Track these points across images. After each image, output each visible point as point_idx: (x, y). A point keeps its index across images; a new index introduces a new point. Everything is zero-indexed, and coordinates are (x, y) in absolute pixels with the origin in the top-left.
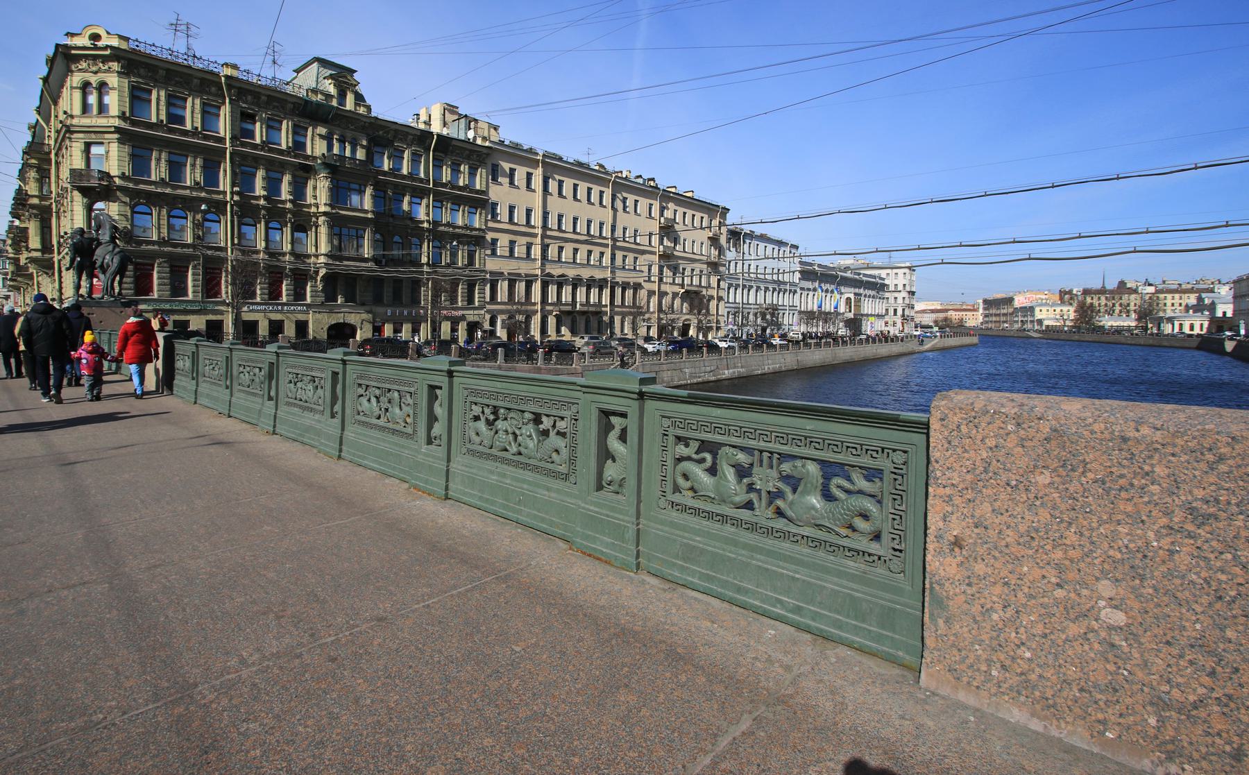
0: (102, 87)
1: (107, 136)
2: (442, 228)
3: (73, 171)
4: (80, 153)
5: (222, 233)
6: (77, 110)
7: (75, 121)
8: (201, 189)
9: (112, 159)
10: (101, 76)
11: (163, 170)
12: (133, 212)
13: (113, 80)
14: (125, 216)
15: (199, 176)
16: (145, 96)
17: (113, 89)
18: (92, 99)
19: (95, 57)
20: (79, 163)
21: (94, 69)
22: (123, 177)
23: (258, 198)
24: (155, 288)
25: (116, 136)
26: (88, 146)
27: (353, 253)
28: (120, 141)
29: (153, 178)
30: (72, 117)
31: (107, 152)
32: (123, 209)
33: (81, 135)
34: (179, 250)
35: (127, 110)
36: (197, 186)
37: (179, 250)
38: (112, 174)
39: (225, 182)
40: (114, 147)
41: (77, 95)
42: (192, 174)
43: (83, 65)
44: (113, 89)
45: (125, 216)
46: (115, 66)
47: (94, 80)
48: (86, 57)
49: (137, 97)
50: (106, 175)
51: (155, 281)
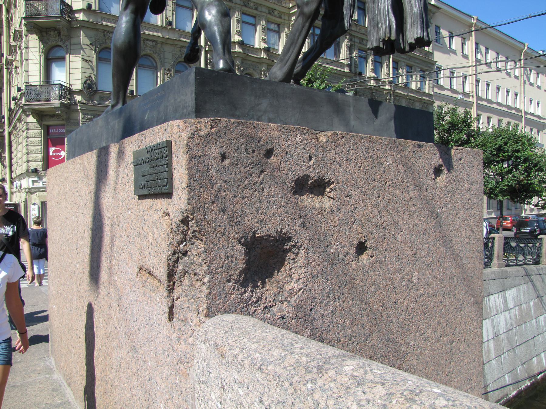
38: (75, 8)
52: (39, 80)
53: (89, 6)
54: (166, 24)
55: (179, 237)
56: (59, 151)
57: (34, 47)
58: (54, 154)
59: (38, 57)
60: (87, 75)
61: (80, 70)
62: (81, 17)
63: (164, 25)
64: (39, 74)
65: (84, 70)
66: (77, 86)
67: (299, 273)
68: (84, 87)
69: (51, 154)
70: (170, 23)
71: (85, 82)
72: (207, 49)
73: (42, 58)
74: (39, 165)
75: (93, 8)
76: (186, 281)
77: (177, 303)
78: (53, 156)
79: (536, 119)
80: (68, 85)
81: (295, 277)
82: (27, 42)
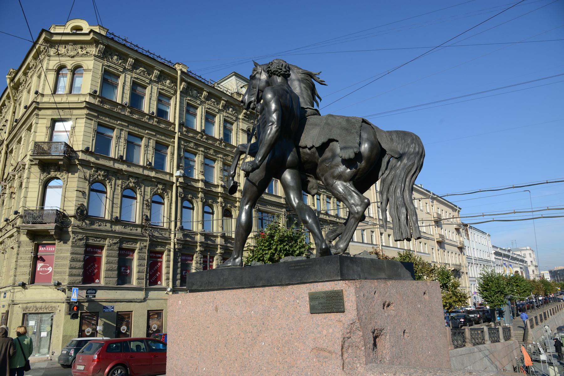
0: (76, 69)
1: (75, 112)
2: (321, 216)
3: (37, 145)
4: (45, 130)
5: (165, 214)
6: (48, 91)
7: (45, 99)
8: (152, 169)
9: (74, 133)
10: (78, 60)
11: (121, 148)
12: (91, 190)
13: (89, 63)
14: (84, 193)
15: (151, 157)
16: (113, 80)
17: (88, 70)
18: (64, 82)
19: (75, 43)
20: (41, 135)
21: (72, 54)
22: (87, 151)
23: (197, 181)
24: (103, 274)
25: (86, 111)
26: (54, 121)
27: (389, 246)
28: (89, 117)
29: (112, 155)
30: (43, 95)
31: (73, 128)
32: (81, 185)
33: (49, 112)
34: (128, 230)
35: (98, 90)
36: (149, 167)
37: (128, 230)
38: (75, 149)
39: (171, 165)
40: (82, 124)
41: (51, 77)
42: (144, 155)
43: (62, 50)
44: (88, 70)
45: (84, 193)
46: (93, 50)
47: (70, 63)
48: (66, 43)
49: (108, 79)
50: (69, 149)
51: (103, 267)
52: (35, 205)
53: (88, 148)
54: (147, 165)
55: (348, 331)
56: (47, 267)
57: (35, 177)
58: (41, 269)
59: (38, 186)
60: (80, 203)
61: (75, 199)
62: (81, 156)
63: (145, 165)
64: (36, 200)
65: (78, 199)
66: (71, 210)
67: (388, 345)
68: (77, 213)
69: (38, 269)
70: (150, 164)
71: (78, 209)
72: (178, 185)
73: (41, 187)
74: (26, 278)
75: (90, 150)
76: (350, 351)
77: (346, 361)
78: (40, 271)
79: (266, 161)
80: (62, 211)
81: (386, 347)
82: (30, 172)
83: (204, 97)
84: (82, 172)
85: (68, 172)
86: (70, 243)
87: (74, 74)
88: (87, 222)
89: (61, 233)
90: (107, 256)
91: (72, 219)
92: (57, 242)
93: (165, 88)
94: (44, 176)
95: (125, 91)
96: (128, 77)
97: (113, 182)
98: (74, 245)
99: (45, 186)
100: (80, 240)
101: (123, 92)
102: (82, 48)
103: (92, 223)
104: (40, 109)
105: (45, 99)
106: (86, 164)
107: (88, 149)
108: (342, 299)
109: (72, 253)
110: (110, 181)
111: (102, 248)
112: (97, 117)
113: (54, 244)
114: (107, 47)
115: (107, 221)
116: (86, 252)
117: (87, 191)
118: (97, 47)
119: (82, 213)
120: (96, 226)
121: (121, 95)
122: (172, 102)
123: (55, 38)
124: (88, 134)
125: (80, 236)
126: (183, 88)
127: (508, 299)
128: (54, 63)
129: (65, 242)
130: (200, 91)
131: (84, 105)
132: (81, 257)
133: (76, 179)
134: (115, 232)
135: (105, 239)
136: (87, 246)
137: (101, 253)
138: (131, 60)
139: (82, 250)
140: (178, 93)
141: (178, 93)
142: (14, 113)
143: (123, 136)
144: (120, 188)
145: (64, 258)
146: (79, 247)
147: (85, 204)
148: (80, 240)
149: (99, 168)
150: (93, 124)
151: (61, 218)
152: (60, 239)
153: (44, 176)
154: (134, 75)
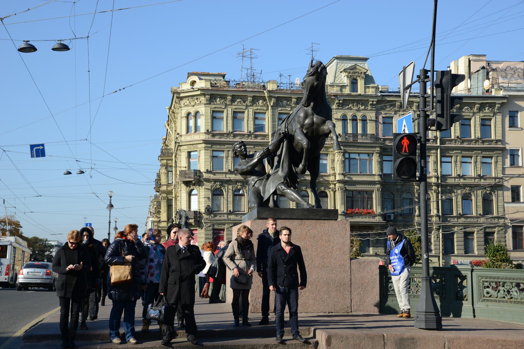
10: (197, 108)
11: (230, 164)
17: (202, 115)
22: (208, 172)
28: (206, 149)
33: (186, 147)
41: (184, 121)
44: (202, 115)
45: (208, 198)
49: (215, 117)
57: (183, 191)
62: (205, 176)
66: (203, 210)
83: (294, 103)
84: (208, 185)
85: (199, 185)
86: (204, 228)
87: (196, 117)
88: (212, 215)
89: (199, 223)
90: (227, 235)
91: (204, 215)
92: (197, 228)
93: (259, 108)
94: (188, 189)
95: (228, 122)
96: (230, 110)
97: (226, 188)
98: (206, 230)
99: (190, 194)
100: (209, 226)
101: (227, 123)
102: (197, 99)
103: (215, 216)
104: (181, 146)
105: (183, 139)
106: (208, 180)
107: (207, 170)
108: (61, 317)
109: (205, 235)
110: (224, 187)
111: (223, 230)
112: (210, 147)
113: (197, 230)
114: (211, 95)
115: (224, 214)
116: (214, 233)
117: (210, 197)
118: (205, 97)
119: (209, 211)
120: (217, 218)
121: (225, 125)
122: (266, 116)
123: (182, 95)
124: (207, 160)
125: (209, 225)
126: (274, 103)
127: (519, 266)
128: (184, 111)
129: (202, 229)
130: (289, 99)
131: (202, 142)
132: (211, 237)
133: (203, 190)
134: (230, 220)
135: (225, 225)
136: (214, 230)
137: (223, 233)
138: (229, 98)
139: (211, 232)
140: (270, 108)
141: (270, 108)
142: (176, 131)
143: (230, 155)
144: (231, 191)
145: (202, 238)
146: (209, 230)
147: (210, 205)
148: (209, 226)
149: (215, 181)
150: (209, 153)
151: (197, 215)
152: (199, 227)
153: (188, 189)
154: (234, 107)
